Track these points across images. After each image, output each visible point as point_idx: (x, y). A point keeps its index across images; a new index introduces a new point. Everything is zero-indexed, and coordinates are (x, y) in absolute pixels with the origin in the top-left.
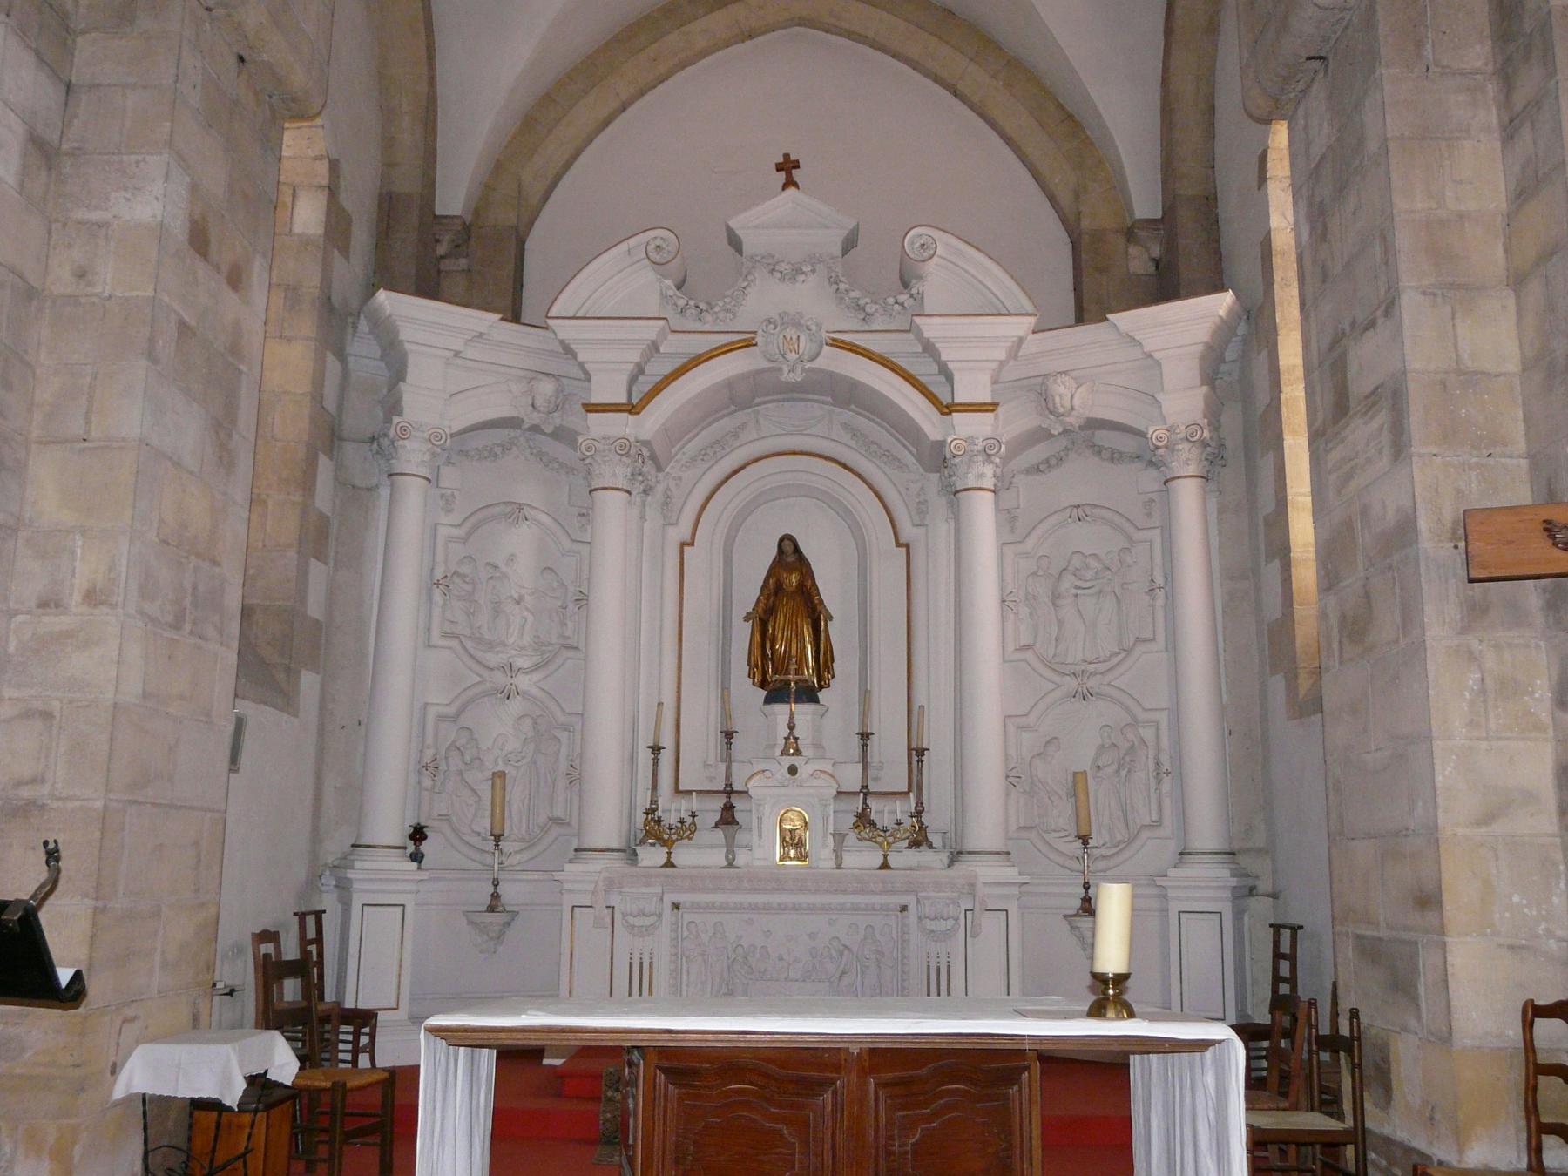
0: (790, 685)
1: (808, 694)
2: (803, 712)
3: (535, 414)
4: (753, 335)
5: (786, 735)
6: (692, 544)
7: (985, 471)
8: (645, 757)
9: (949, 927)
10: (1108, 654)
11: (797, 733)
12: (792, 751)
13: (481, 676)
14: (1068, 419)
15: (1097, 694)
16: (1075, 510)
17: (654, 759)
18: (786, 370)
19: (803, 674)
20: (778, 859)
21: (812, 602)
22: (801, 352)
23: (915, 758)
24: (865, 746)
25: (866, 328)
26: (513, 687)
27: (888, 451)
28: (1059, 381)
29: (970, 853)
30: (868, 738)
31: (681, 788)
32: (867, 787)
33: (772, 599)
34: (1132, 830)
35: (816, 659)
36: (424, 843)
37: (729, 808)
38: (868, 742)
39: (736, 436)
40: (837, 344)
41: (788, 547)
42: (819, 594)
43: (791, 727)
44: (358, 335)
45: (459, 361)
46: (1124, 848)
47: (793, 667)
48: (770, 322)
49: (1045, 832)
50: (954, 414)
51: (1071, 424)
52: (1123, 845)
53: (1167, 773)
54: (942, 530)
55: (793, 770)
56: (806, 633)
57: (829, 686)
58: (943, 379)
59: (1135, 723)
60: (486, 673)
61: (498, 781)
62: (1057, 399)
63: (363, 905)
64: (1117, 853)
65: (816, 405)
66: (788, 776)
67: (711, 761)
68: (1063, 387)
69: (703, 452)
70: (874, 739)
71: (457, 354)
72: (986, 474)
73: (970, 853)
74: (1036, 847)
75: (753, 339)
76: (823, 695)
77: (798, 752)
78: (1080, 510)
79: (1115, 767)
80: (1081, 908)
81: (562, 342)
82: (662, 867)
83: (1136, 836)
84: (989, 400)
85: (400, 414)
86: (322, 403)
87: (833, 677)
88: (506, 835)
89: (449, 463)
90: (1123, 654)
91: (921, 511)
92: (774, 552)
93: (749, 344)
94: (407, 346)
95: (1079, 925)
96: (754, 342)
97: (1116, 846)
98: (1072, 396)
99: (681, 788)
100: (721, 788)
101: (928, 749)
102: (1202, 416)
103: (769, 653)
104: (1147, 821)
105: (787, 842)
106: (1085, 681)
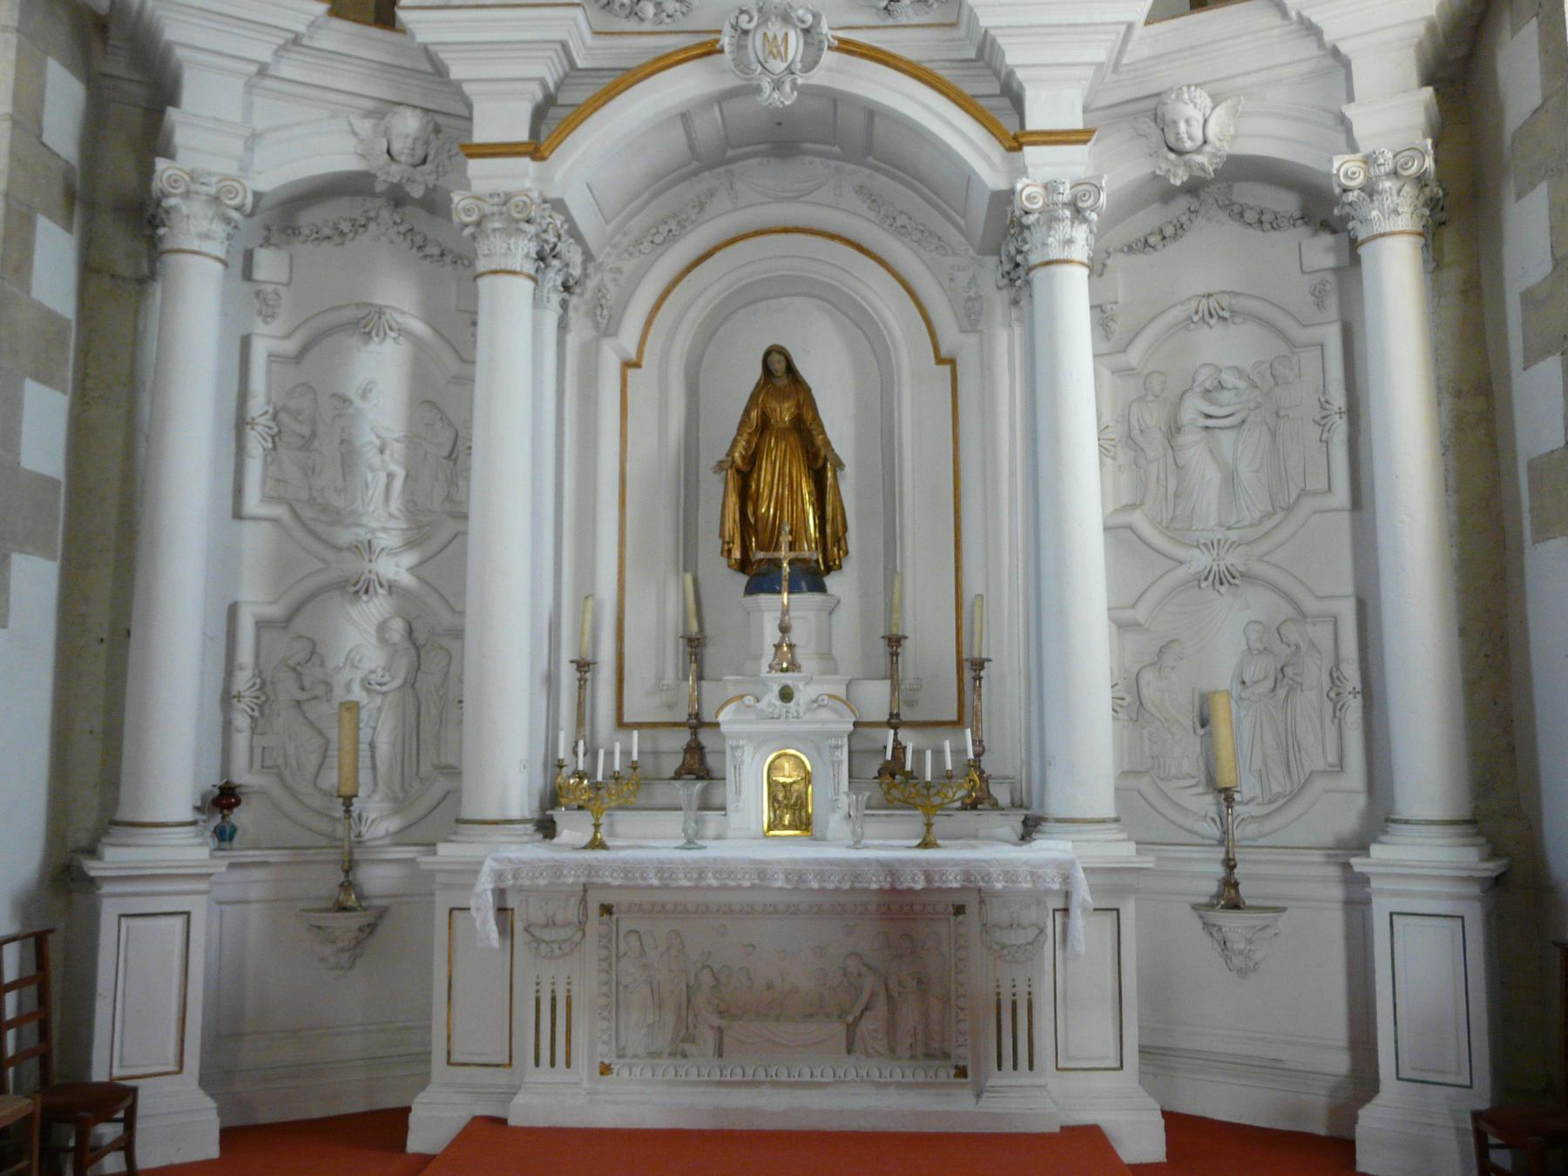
0: (780, 567)
1: (811, 577)
2: (803, 605)
3: (394, 168)
4: (713, 36)
5: (777, 641)
6: (637, 365)
7: (1074, 234)
8: (568, 674)
9: (1030, 940)
10: (1257, 514)
11: (795, 637)
12: (785, 665)
13: (324, 561)
14: (1199, 158)
15: (1242, 575)
16: (1204, 301)
17: (580, 680)
18: (767, 86)
19: (801, 549)
20: (766, 827)
21: (813, 444)
22: (790, 58)
23: (968, 675)
24: (895, 655)
25: (890, 22)
26: (373, 577)
27: (923, 225)
28: (1186, 96)
29: (1058, 820)
30: (982, 667)
31: (626, 720)
32: (898, 715)
33: (755, 440)
34: (1296, 778)
35: (821, 527)
36: (236, 810)
37: (695, 750)
38: (983, 673)
39: (701, 207)
40: (847, 48)
41: (778, 365)
42: (823, 432)
43: (784, 629)
44: (111, 42)
45: (268, 83)
46: (1283, 805)
47: (785, 539)
48: (742, 12)
49: (1162, 779)
50: (1026, 149)
51: (1202, 168)
52: (1281, 802)
53: (1350, 693)
54: (1005, 341)
55: (786, 695)
56: (805, 491)
57: (840, 567)
58: (1006, 102)
59: (1302, 615)
60: (328, 554)
61: (347, 716)
62: (1182, 127)
63: (121, 916)
64: (1275, 811)
65: (817, 160)
66: (778, 703)
67: (670, 675)
68: (1191, 106)
69: (654, 231)
70: (908, 645)
71: (263, 71)
72: (1079, 241)
73: (1058, 820)
74: (1150, 804)
75: (717, 41)
76: (831, 581)
77: (794, 666)
78: (1211, 300)
79: (1270, 683)
80: (1218, 896)
81: (425, 50)
82: (585, 848)
83: (1302, 788)
84: (1079, 126)
85: (169, 153)
86: (39, 137)
87: (846, 553)
88: (360, 794)
89: (267, 242)
90: (1280, 516)
91: (972, 317)
92: (756, 372)
93: (710, 50)
94: (179, 52)
95: (1220, 922)
96: (718, 46)
97: (1271, 802)
98: (1205, 121)
99: (626, 720)
100: (684, 718)
101: (989, 660)
102: (1420, 133)
103: (752, 520)
104: (1320, 765)
105: (778, 801)
106: (1222, 554)
